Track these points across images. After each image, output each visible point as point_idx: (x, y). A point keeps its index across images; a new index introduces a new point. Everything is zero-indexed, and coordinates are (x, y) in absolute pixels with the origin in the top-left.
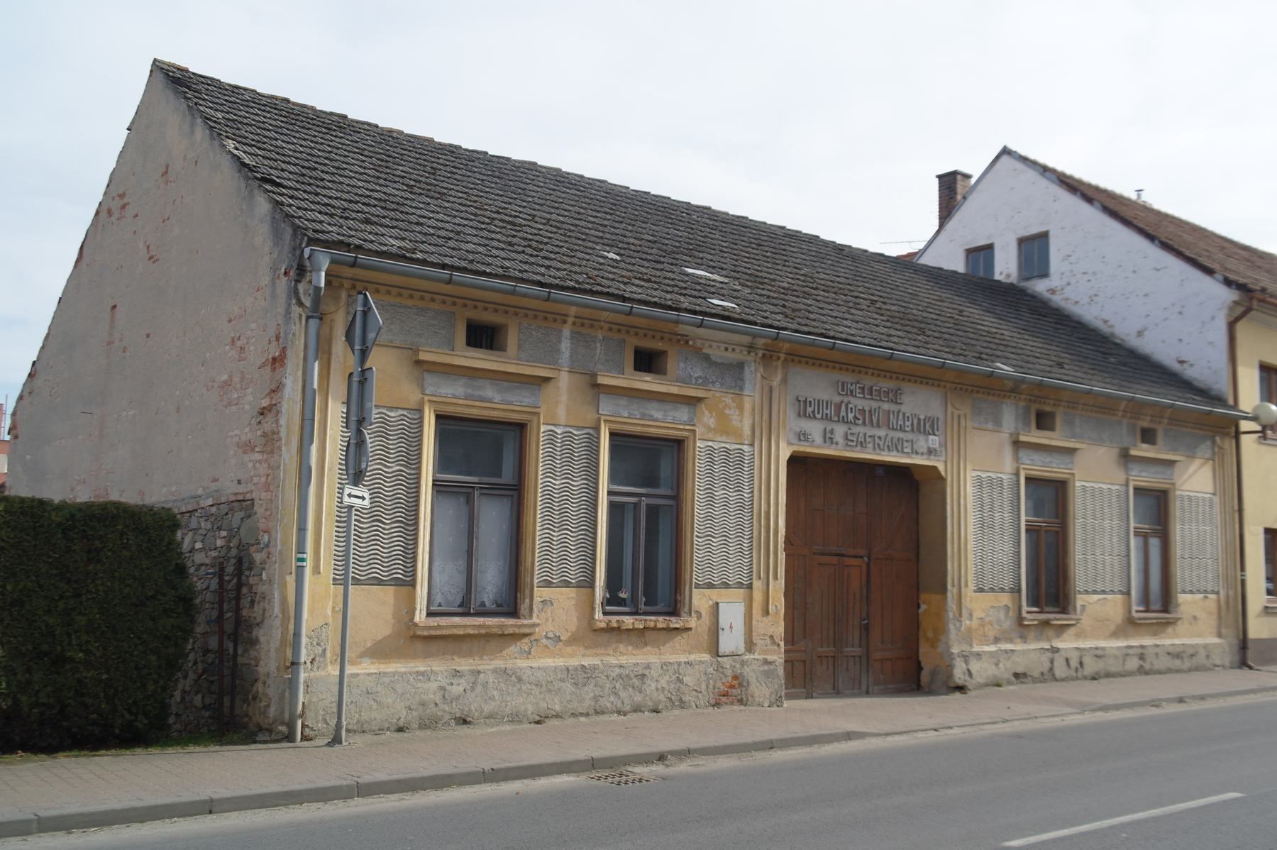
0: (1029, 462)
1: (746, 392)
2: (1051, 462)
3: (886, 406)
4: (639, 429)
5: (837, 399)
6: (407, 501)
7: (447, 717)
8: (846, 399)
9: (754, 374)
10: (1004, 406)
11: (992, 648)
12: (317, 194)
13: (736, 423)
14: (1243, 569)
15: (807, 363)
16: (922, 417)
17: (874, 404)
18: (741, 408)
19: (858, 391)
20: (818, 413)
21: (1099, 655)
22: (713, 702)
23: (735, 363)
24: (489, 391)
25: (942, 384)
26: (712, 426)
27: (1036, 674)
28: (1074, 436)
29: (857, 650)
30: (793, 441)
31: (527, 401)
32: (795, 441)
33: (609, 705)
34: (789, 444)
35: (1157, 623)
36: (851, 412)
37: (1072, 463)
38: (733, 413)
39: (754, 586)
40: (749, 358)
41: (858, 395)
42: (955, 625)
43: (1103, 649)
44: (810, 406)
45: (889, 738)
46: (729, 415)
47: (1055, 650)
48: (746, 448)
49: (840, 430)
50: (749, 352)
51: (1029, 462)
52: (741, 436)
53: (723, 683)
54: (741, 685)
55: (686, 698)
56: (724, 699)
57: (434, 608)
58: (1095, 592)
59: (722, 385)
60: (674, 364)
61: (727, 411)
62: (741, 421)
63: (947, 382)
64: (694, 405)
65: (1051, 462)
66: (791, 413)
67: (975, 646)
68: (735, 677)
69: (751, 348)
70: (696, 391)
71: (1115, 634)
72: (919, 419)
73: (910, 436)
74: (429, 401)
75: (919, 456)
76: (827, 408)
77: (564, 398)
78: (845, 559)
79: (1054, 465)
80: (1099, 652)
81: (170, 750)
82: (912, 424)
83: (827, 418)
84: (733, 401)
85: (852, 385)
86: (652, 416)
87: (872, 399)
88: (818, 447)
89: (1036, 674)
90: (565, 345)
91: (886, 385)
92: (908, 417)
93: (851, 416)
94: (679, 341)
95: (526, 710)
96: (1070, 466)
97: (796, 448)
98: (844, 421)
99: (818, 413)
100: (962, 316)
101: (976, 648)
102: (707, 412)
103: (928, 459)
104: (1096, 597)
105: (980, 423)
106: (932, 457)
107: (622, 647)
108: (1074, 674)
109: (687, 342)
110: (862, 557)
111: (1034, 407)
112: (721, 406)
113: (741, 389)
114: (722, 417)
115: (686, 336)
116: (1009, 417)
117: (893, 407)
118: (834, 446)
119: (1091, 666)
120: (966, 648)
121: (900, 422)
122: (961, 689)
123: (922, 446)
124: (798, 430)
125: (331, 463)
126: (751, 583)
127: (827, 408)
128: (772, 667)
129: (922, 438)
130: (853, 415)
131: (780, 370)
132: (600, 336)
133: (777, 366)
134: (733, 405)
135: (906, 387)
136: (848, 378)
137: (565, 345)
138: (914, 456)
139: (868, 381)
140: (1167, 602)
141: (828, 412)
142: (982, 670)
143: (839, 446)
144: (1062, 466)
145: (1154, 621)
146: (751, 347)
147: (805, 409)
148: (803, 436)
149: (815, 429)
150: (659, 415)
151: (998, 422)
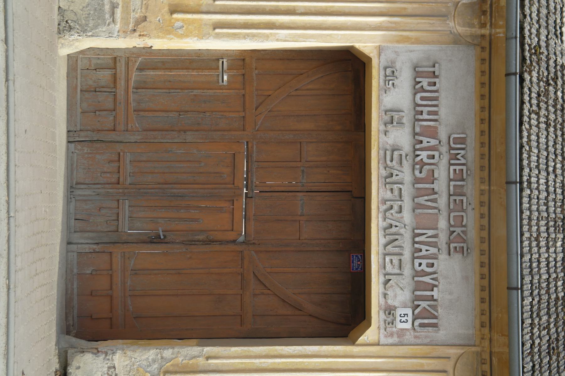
5: (443, 135)
8: (444, 149)
16: (435, 293)
20: (422, 99)
25: (486, 330)
42: (154, 361)
75: (382, 289)
88: (380, 101)
91: (473, 234)
92: (435, 84)
103: (380, 306)
117: (443, 238)
118: (382, 128)
124: (398, 65)
130: (426, 160)
135: (474, 257)
141: (425, 116)
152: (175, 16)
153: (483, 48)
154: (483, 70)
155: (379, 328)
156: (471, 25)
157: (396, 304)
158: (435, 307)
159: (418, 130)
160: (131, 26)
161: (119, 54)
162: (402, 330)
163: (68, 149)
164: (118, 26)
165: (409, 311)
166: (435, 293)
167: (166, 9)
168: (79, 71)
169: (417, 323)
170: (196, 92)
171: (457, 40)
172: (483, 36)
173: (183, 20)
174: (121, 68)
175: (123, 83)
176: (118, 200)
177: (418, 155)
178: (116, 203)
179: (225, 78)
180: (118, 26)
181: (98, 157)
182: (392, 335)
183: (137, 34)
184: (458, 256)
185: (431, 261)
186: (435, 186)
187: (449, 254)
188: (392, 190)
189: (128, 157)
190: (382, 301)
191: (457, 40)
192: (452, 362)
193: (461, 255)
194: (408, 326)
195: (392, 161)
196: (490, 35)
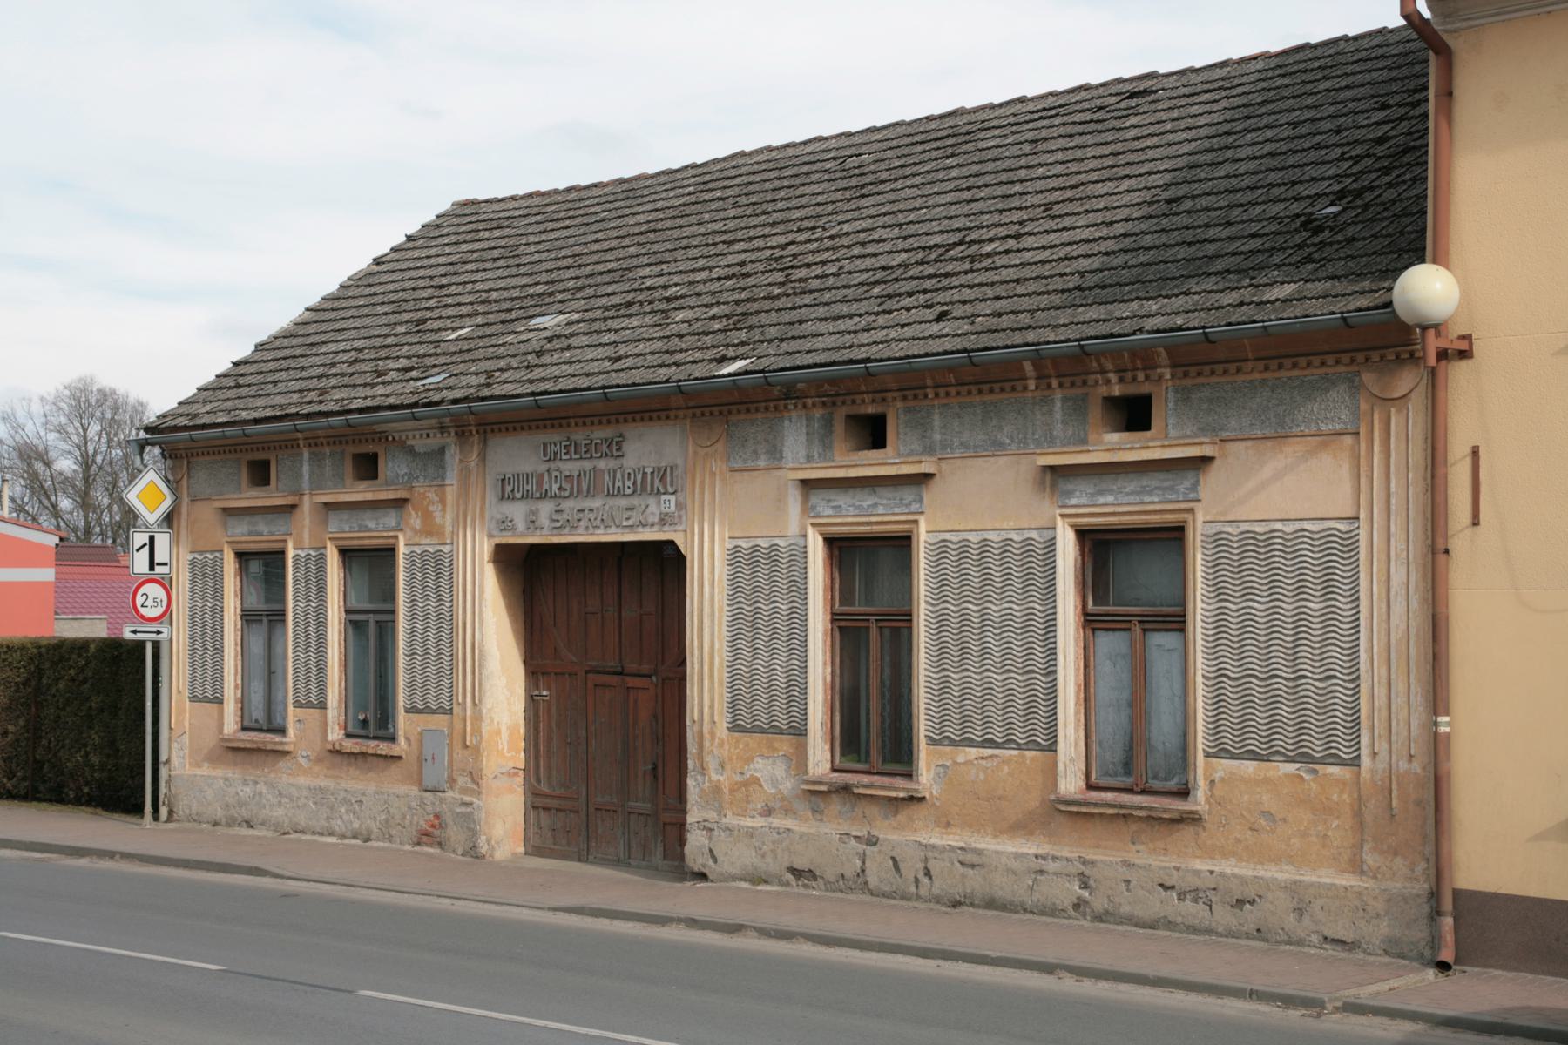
0: (830, 512)
1: (448, 482)
2: (876, 505)
3: (602, 464)
4: (381, 541)
5: (543, 467)
6: (969, 620)
7: (240, 819)
8: (553, 465)
9: (453, 457)
10: (787, 423)
11: (759, 822)
12: (751, 239)
13: (438, 520)
14: (1437, 697)
15: (507, 429)
16: (649, 470)
17: (587, 465)
18: (443, 501)
19: (563, 451)
20: (518, 491)
21: (972, 861)
22: (415, 840)
23: (437, 449)
24: (262, 527)
25: (672, 414)
26: (418, 528)
27: (830, 874)
28: (929, 450)
29: (646, 807)
30: (495, 533)
31: (283, 529)
32: (495, 533)
33: (337, 828)
34: (490, 536)
35: (1149, 818)
36: (556, 482)
37: (921, 501)
38: (435, 509)
39: (454, 712)
40: (448, 440)
41: (564, 457)
42: (696, 780)
43: (979, 852)
44: (509, 483)
45: (487, 906)
46: (432, 512)
47: (872, 841)
48: (446, 549)
49: (546, 508)
50: (442, 433)
51: (830, 512)
52: (443, 534)
53: (426, 821)
54: (441, 827)
55: (393, 832)
56: (425, 839)
57: (246, 723)
58: (969, 743)
59: (425, 477)
60: (388, 467)
61: (431, 508)
62: (443, 517)
63: (758, 402)
64: (401, 507)
65: (876, 505)
66: (491, 496)
67: (729, 814)
68: (437, 816)
69: (442, 429)
70: (385, 493)
71: (1023, 827)
72: (645, 474)
73: (635, 501)
74: (227, 542)
75: (647, 529)
76: (528, 483)
77: (307, 522)
78: (628, 679)
79: (881, 510)
80: (969, 858)
81: (116, 816)
82: (635, 483)
83: (526, 496)
84: (437, 495)
85: (555, 445)
86: (366, 526)
87: (581, 458)
88: (521, 535)
89: (830, 874)
90: (306, 468)
91: (599, 434)
92: (629, 474)
93: (555, 487)
94: (380, 439)
95: (284, 822)
96: (914, 507)
97: (498, 541)
98: (545, 496)
99: (518, 491)
100: (1053, 217)
101: (730, 820)
102: (413, 513)
103: (660, 530)
104: (973, 752)
105: (745, 461)
106: (666, 528)
107: (352, 770)
108: (913, 889)
109: (387, 439)
110: (650, 676)
111: (841, 413)
112: (425, 503)
113: (443, 479)
114: (427, 516)
115: (385, 432)
116: (795, 438)
117: (612, 463)
118: (538, 532)
119: (948, 880)
120: (711, 815)
121: (618, 484)
122: (702, 876)
123: (653, 513)
124: (499, 517)
125: (720, 577)
126: (452, 709)
127: (528, 483)
128: (468, 810)
129: (652, 501)
130: (558, 485)
131: (476, 447)
132: (328, 452)
133: (473, 442)
134: (436, 499)
135: (630, 430)
136: (554, 437)
137: (306, 468)
138: (640, 529)
139: (579, 436)
140: (900, 754)
141: (530, 488)
142: (735, 857)
143: (545, 531)
144: (896, 510)
145: (1110, 811)
146: (442, 427)
147: (508, 490)
148: (505, 524)
149: (517, 512)
150: (371, 524)
151: (775, 453)
152: (468, 743)
153: (730, 412)
154: (1182, 375)
155: (675, 531)
156: (472, 446)
157: (658, 513)
158: (659, 469)
159: (538, 495)
160: (476, 788)
161: (529, 803)
162: (676, 505)
163: (592, 863)
164: (474, 800)
165: (664, 497)
166: (649, 470)
167: (465, 751)
168: (556, 847)
169: (670, 490)
170: (554, 725)
171: (483, 458)
172: (478, 432)
173: (471, 735)
174: (539, 802)
175: (548, 801)
176: (630, 813)
177: (658, 490)
178: (632, 816)
179: (545, 693)
180: (474, 800)
181: (600, 831)
182: (680, 517)
183: (480, 782)
184: (625, 446)
185: (626, 476)
186: (575, 474)
187: (622, 456)
188: (579, 520)
189: (599, 799)
190: (656, 528)
191: (483, 458)
192: (699, 449)
193: (624, 444)
194: (673, 498)
195: (558, 521)
196: (476, 426)
